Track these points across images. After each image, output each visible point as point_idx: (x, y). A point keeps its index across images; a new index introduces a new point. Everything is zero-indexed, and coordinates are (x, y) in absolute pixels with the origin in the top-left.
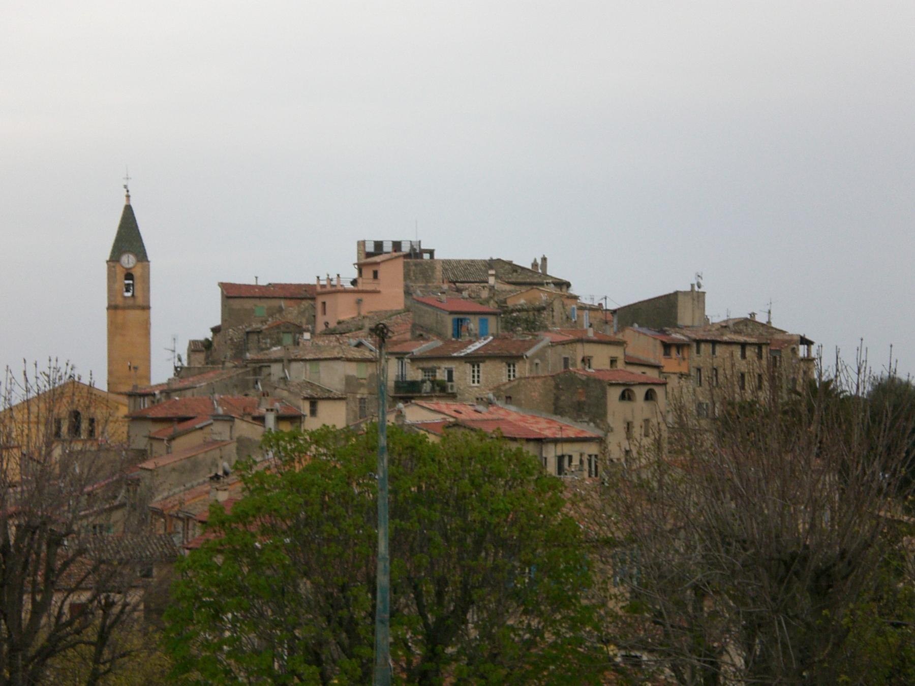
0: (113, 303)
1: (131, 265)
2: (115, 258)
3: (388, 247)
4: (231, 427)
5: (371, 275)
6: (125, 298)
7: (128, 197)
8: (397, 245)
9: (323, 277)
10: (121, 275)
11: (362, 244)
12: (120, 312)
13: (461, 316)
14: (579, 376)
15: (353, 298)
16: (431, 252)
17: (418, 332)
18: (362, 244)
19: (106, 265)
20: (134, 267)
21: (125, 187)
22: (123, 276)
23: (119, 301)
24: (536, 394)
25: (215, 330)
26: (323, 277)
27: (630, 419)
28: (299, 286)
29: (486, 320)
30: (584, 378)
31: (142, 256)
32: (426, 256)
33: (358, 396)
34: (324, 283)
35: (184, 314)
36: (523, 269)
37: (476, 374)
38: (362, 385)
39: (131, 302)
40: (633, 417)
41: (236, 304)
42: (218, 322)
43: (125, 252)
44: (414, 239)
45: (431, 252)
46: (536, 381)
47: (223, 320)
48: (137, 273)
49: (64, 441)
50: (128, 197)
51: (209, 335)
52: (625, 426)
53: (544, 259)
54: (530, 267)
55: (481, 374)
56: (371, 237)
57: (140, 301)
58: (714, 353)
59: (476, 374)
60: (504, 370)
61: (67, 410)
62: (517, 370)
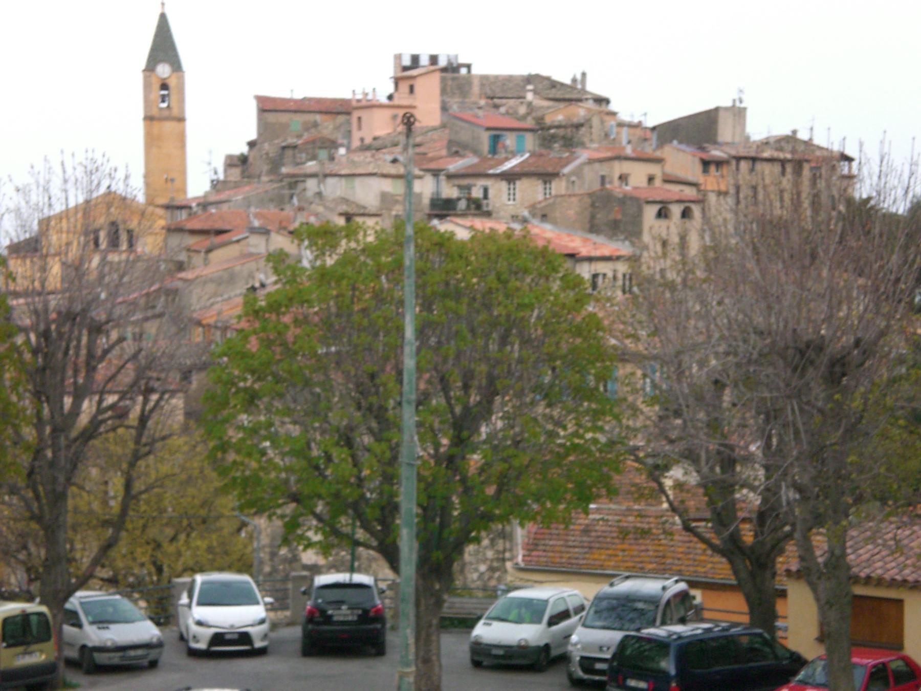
0: (149, 114)
1: (166, 76)
2: (150, 68)
3: (424, 61)
5: (407, 90)
6: (162, 109)
11: (398, 57)
12: (156, 123)
16: (469, 66)
17: (454, 149)
23: (155, 112)
25: (252, 144)
31: (177, 66)
32: (464, 71)
36: (562, 85)
38: (397, 202)
39: (166, 113)
41: (272, 118)
42: (253, 135)
43: (160, 61)
44: (452, 53)
45: (469, 66)
47: (260, 134)
48: (172, 83)
51: (245, 149)
57: (175, 112)
61: (105, 223)
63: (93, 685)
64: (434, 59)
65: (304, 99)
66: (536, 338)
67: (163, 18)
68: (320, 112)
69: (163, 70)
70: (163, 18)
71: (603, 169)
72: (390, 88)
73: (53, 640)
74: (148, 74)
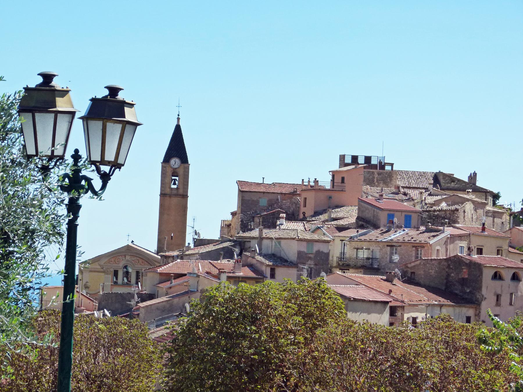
0: (163, 192)
1: (176, 166)
2: (167, 160)
3: (361, 160)
6: (172, 189)
7: (178, 119)
8: (368, 159)
9: (306, 180)
11: (342, 158)
12: (167, 198)
13: (392, 213)
14: (465, 260)
16: (392, 165)
17: (361, 223)
19: (161, 165)
20: (179, 167)
22: (171, 174)
23: (168, 191)
24: (433, 271)
25: (233, 214)
26: (306, 180)
27: (499, 292)
28: (480, 187)
30: (468, 262)
31: (184, 159)
32: (388, 168)
34: (307, 184)
36: (459, 180)
38: (310, 258)
40: (502, 291)
42: (235, 208)
43: (174, 157)
44: (380, 155)
45: (392, 165)
48: (181, 172)
49: (378, 262)
50: (178, 119)
51: (229, 217)
52: (495, 298)
53: (330, 172)
54: (466, 180)
56: (349, 154)
64: (368, 159)
69: (175, 162)
71: (31, 274)
72: (81, 202)
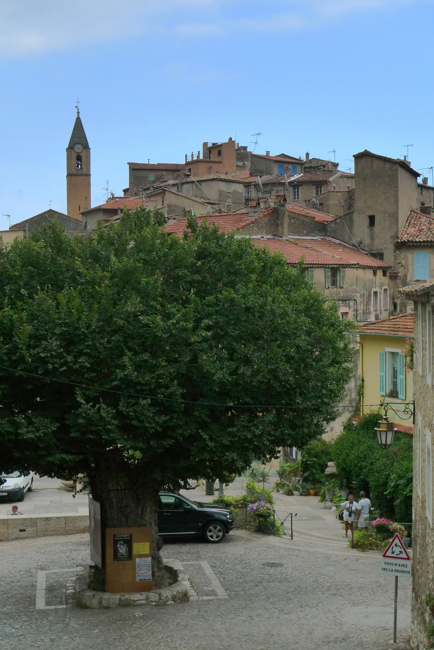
0: (70, 172)
1: (80, 151)
2: (70, 148)
4: (163, 198)
5: (217, 153)
7: (78, 113)
10: (74, 156)
11: (205, 144)
12: (74, 177)
15: (206, 165)
18: (205, 144)
21: (76, 107)
23: (74, 171)
25: (125, 191)
29: (296, 167)
31: (86, 147)
33: (227, 204)
35: (108, 183)
37: (296, 193)
39: (79, 172)
41: (138, 174)
42: (127, 186)
46: (338, 194)
47: (131, 183)
48: (83, 155)
50: (78, 113)
55: (300, 193)
57: (84, 171)
58: (421, 193)
59: (296, 193)
60: (314, 191)
61: (44, 225)
62: (322, 190)
63: (263, 537)
65: (158, 164)
66: (174, 302)
67: (78, 121)
68: (166, 170)
70: (78, 121)
73: (6, 479)
74: (69, 150)
